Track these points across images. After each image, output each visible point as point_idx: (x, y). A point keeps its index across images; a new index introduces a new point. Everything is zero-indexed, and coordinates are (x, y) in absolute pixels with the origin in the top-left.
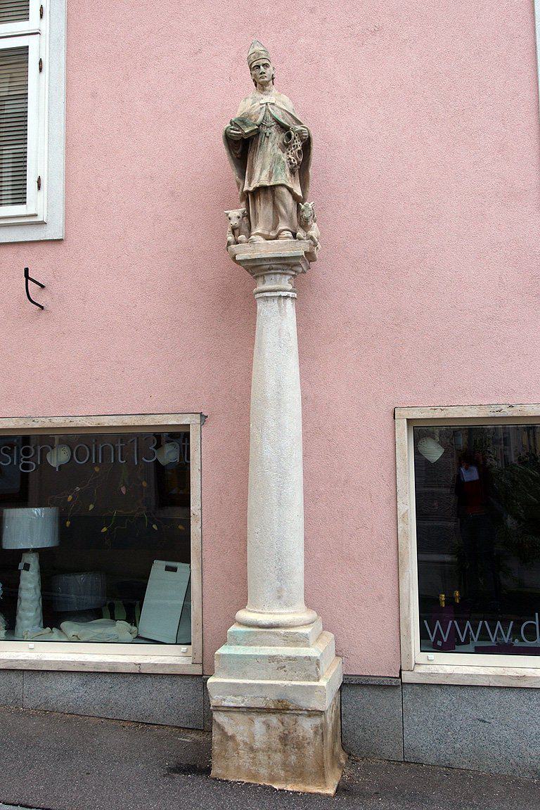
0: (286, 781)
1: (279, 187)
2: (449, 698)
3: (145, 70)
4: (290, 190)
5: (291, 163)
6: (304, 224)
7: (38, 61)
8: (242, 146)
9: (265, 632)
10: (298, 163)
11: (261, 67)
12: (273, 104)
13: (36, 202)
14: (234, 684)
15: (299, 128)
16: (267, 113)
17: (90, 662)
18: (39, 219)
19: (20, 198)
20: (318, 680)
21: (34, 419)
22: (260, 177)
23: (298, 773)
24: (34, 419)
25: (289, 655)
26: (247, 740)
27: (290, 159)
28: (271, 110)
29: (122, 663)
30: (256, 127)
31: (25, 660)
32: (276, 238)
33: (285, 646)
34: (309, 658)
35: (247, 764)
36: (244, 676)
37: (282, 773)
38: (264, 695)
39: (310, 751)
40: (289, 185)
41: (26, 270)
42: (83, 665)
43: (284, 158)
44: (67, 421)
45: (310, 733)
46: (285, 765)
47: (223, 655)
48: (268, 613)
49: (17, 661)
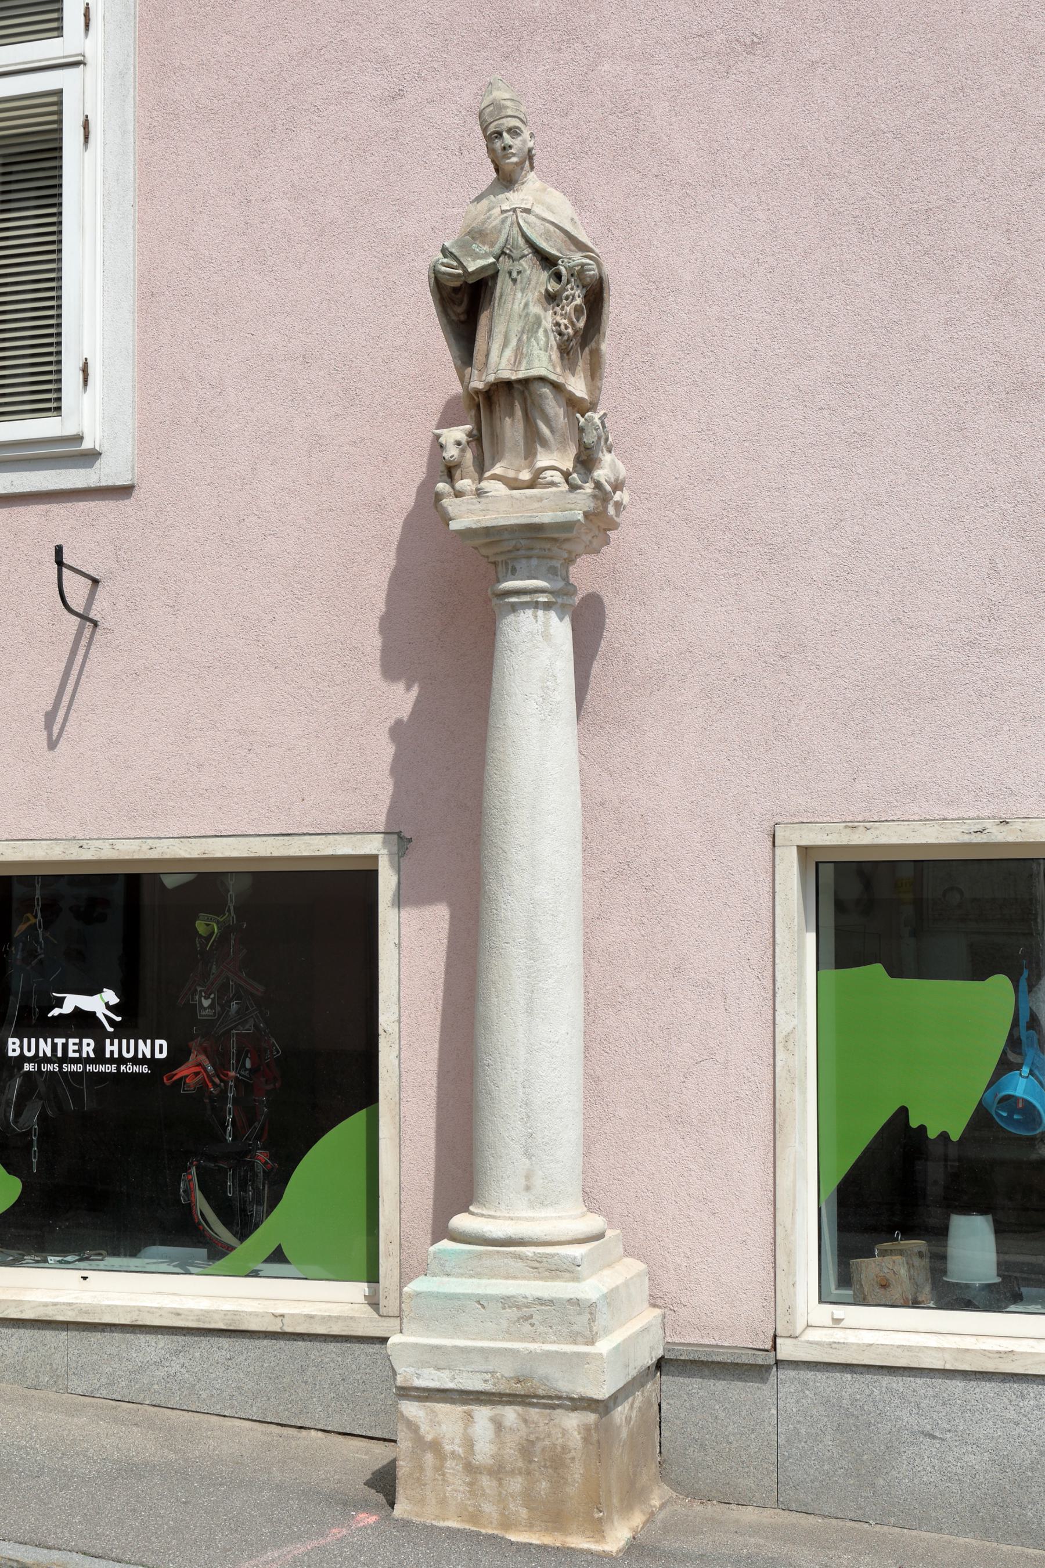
0: (530, 1526)
1: (536, 383)
2: (867, 1392)
3: (292, 135)
4: (557, 388)
5: (560, 334)
6: (586, 461)
7: (81, 119)
8: (465, 303)
9: (498, 1252)
10: (576, 332)
11: (505, 134)
12: (527, 211)
13: (86, 411)
14: (438, 1347)
15: (578, 258)
16: (516, 229)
17: (191, 1311)
18: (87, 445)
19: (50, 403)
20: (593, 1343)
21: (81, 843)
22: (499, 361)
23: (555, 1518)
24: (81, 843)
25: (539, 1294)
26: (460, 1451)
27: (558, 324)
28: (522, 223)
29: (250, 1313)
30: (492, 260)
31: (70, 1304)
32: (532, 485)
33: (536, 1278)
34: (576, 1302)
35: (460, 1496)
36: (458, 1330)
37: (524, 1513)
38: (491, 1368)
39: (576, 1471)
40: (553, 377)
41: (59, 551)
42: (178, 1314)
43: (548, 322)
44: (145, 847)
45: (576, 1439)
46: (528, 1497)
47: (418, 1294)
48: (505, 1218)
49: (55, 1304)
